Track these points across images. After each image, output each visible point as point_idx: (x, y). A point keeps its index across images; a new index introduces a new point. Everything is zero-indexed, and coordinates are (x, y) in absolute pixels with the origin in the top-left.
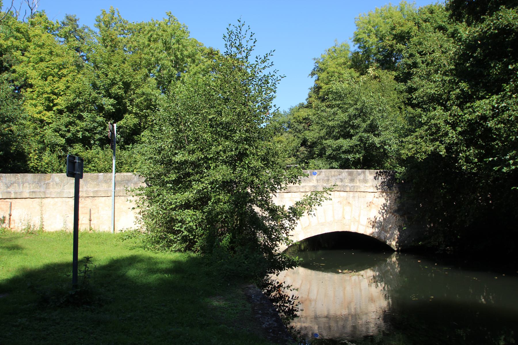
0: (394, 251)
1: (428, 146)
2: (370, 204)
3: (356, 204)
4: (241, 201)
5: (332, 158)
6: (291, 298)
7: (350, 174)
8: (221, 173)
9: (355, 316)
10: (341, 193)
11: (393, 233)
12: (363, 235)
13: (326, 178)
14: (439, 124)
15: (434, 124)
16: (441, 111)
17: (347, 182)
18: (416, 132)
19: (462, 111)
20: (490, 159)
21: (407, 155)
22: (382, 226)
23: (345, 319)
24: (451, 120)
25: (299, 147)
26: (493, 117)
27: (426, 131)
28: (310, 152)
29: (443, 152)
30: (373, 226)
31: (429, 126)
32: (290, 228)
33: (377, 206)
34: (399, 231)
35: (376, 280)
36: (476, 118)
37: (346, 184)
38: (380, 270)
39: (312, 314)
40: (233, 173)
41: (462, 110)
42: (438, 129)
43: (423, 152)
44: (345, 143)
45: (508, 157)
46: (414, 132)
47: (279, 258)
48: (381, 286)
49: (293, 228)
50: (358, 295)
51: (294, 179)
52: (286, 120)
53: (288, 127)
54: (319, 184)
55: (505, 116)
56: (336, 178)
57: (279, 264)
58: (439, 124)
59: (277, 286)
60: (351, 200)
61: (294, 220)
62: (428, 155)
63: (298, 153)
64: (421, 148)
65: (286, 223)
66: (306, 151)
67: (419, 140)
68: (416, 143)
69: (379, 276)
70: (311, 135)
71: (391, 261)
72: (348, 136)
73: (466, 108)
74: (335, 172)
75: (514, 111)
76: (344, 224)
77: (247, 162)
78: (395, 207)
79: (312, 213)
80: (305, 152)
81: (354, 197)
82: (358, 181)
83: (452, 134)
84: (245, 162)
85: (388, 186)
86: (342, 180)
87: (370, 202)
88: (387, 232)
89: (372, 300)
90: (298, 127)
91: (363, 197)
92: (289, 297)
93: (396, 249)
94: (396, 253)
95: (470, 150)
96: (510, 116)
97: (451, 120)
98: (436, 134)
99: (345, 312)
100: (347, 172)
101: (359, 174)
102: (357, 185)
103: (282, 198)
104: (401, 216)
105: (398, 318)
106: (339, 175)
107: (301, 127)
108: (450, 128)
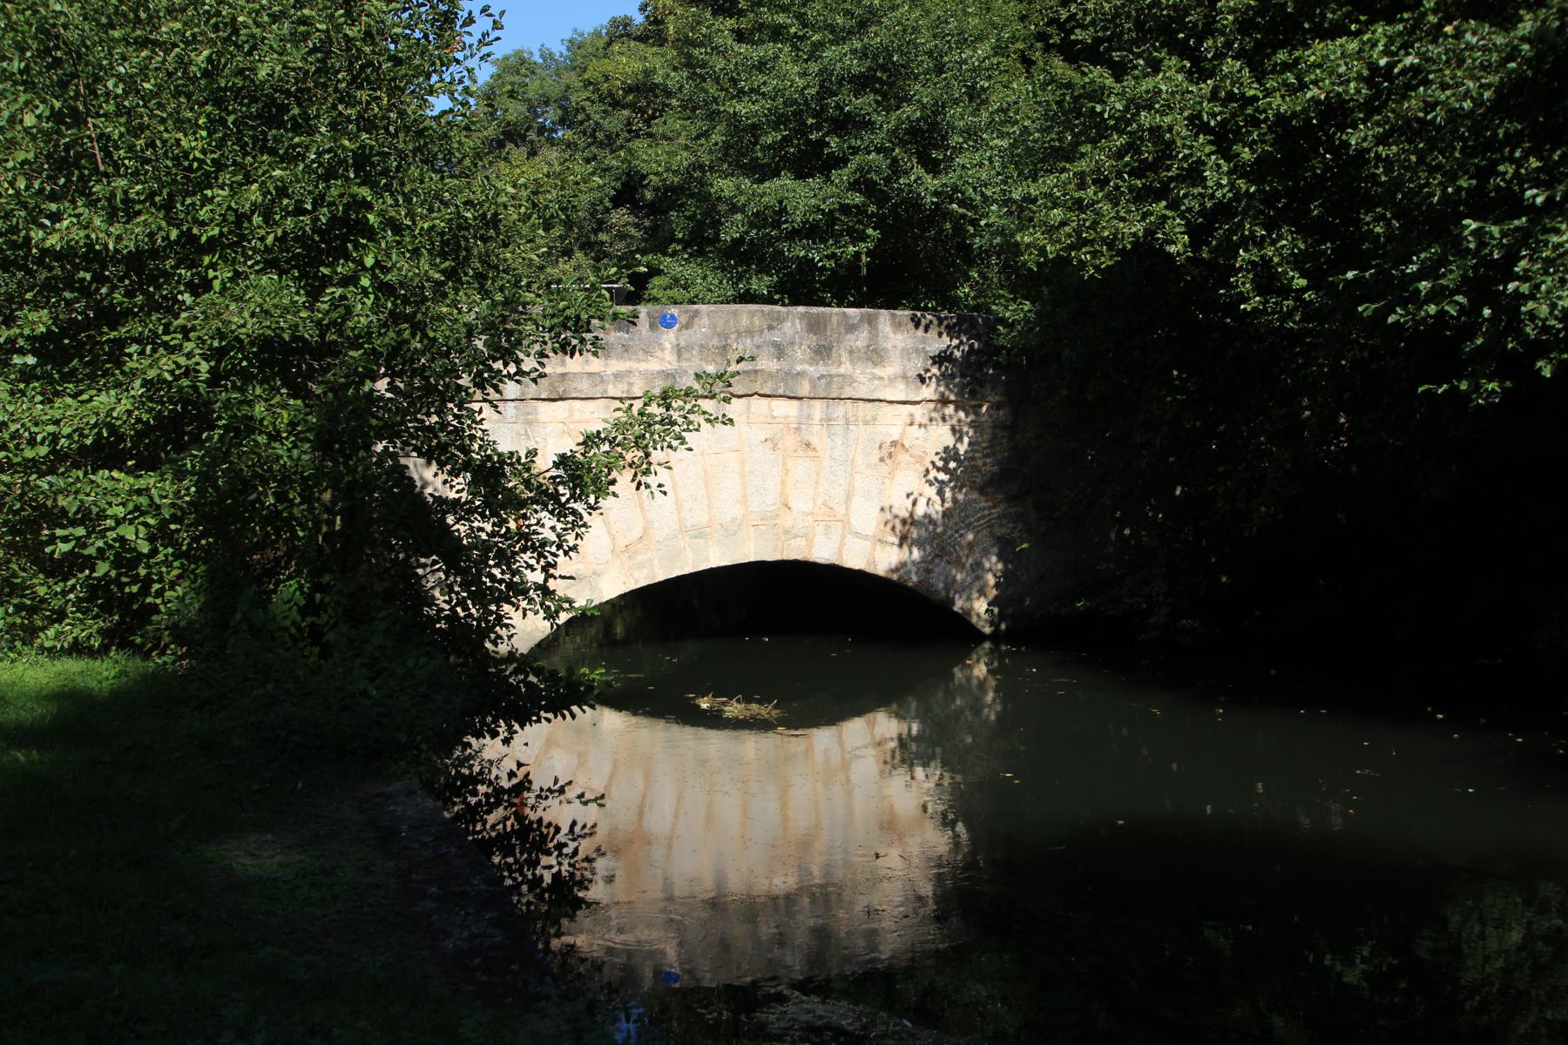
0: (980, 637)
1: (1123, 220)
2: (892, 451)
3: (828, 450)
4: (344, 429)
7: (815, 326)
10: (775, 402)
11: (978, 565)
12: (860, 573)
13: (715, 342)
15: (1151, 130)
16: (1180, 77)
19: (1259, 81)
20: (1350, 275)
24: (1214, 115)
25: (607, 210)
27: (1119, 155)
30: (903, 539)
32: (559, 547)
33: (920, 459)
35: (908, 754)
38: (924, 715)
42: (1166, 150)
43: (1104, 240)
44: (801, 196)
46: (1071, 160)
49: (574, 548)
51: (571, 333)
54: (685, 364)
55: (1412, 104)
58: (1170, 129)
60: (817, 435)
61: (574, 512)
64: (1095, 223)
65: (546, 525)
66: (637, 226)
67: (1091, 191)
68: (1079, 201)
70: (660, 157)
71: (969, 679)
73: (1273, 71)
74: (752, 314)
76: (786, 532)
77: (369, 261)
78: (988, 466)
79: (651, 479)
80: (633, 231)
81: (827, 421)
82: (845, 357)
84: (361, 263)
86: (780, 351)
87: (894, 444)
90: (605, 123)
91: (866, 423)
93: (987, 630)
94: (987, 645)
95: (1280, 237)
98: (1153, 171)
99: (783, 882)
100: (803, 316)
101: (851, 328)
102: (842, 370)
103: (530, 423)
106: (770, 328)
107: (615, 122)
108: (1208, 149)
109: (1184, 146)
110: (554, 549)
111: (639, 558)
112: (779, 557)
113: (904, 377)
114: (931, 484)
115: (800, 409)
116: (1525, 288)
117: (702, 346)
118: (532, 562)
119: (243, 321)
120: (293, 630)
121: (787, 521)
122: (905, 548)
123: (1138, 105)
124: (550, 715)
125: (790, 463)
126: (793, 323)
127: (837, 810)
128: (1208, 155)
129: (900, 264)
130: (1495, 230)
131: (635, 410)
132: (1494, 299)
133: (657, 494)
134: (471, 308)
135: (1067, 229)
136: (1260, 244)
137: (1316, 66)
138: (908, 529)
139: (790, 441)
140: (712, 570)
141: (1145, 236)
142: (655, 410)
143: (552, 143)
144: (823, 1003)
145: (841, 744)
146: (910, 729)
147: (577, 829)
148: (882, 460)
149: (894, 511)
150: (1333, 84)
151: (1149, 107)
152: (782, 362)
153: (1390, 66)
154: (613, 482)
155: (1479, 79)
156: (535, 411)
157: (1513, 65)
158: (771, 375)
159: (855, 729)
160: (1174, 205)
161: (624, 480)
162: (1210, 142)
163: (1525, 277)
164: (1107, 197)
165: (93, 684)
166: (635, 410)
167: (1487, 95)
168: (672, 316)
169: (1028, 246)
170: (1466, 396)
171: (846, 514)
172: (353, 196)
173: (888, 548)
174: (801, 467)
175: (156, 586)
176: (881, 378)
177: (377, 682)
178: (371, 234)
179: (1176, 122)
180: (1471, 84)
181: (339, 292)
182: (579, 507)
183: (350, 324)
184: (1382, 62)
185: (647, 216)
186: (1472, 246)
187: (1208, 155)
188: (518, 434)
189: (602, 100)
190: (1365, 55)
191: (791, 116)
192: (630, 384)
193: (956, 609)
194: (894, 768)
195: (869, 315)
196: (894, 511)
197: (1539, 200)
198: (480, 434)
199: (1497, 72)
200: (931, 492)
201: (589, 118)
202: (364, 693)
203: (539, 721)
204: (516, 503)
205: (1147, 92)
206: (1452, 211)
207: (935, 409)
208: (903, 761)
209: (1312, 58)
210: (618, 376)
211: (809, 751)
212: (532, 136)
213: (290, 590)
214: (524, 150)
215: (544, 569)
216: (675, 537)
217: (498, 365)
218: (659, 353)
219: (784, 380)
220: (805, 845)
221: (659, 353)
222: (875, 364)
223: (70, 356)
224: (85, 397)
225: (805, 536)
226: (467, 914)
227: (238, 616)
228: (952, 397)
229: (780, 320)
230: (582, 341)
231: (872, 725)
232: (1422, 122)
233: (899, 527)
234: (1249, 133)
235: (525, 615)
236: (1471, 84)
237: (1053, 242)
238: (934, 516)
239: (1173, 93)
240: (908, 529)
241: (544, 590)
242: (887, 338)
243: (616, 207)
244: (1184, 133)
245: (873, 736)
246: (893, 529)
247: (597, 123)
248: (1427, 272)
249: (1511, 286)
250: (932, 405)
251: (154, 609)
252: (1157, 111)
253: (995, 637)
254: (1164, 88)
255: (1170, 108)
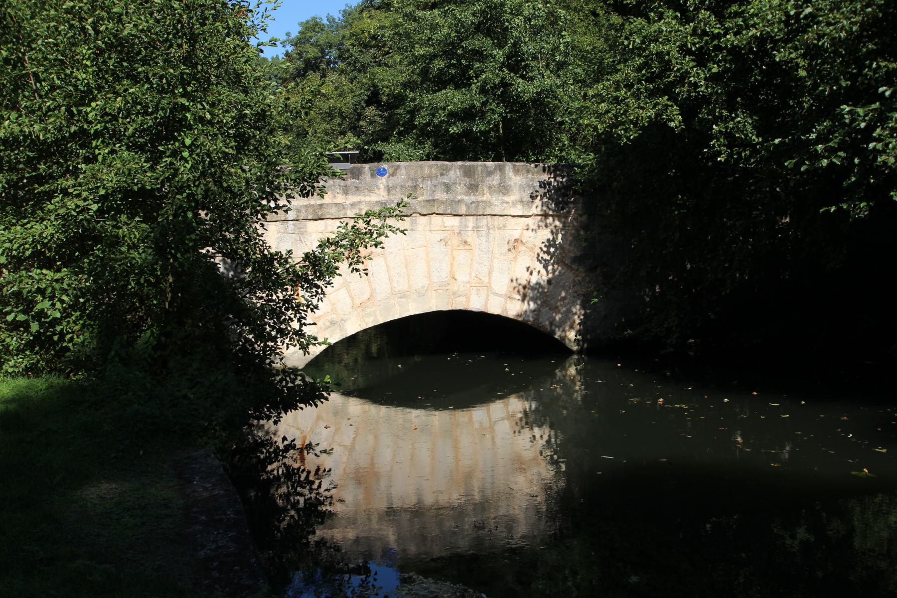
0: (570, 352)
1: (642, 108)
2: (515, 245)
3: (477, 245)
4: (175, 240)
5: (424, 133)
6: (313, 473)
7: (468, 173)
8: (116, 168)
9: (483, 506)
10: (446, 218)
11: (569, 311)
12: (498, 316)
13: (410, 183)
14: (668, 53)
15: (658, 54)
16: (674, 22)
17: (460, 193)
18: (617, 71)
19: (721, 23)
20: (777, 141)
21: (595, 129)
22: (541, 295)
23: (458, 512)
24: (694, 44)
25: (363, 108)
26: (786, 41)
27: (639, 69)
28: (388, 119)
29: (676, 122)
30: (524, 297)
31: (646, 57)
32: (308, 306)
33: (532, 249)
34: (583, 307)
35: (529, 420)
36: (749, 43)
37: (459, 198)
38: (538, 398)
39: (382, 505)
40: (152, 169)
41: (721, 18)
42: (666, 66)
43: (631, 121)
44: (454, 98)
45: (813, 136)
46: (611, 73)
47: (281, 381)
48: (542, 434)
49: (316, 307)
50: (492, 453)
51: (307, 183)
52: (335, 38)
53: (340, 57)
54: (392, 197)
55: (810, 36)
56: (434, 182)
57: (305, 391)
58: (668, 53)
59: (281, 447)
60: (470, 236)
61: (318, 287)
62: (643, 128)
63: (362, 123)
64: (626, 111)
65: (302, 295)
66: (381, 116)
67: (623, 92)
68: (617, 98)
69: (537, 411)
70: (391, 76)
71: (565, 376)
72: (461, 81)
73: (730, 17)
74: (431, 167)
75: (829, 24)
76: (454, 294)
77: (188, 142)
78: (575, 252)
79: (360, 266)
80: (378, 119)
81: (477, 228)
82: (486, 190)
83: (698, 76)
84: (183, 143)
85: (559, 199)
86: (448, 188)
87: (516, 241)
88: (556, 309)
89: (519, 464)
90: (361, 58)
91: (499, 229)
92: (309, 472)
93: (575, 348)
94: (575, 357)
95: (737, 116)
96: (820, 37)
97: (694, 44)
98: (659, 79)
99: (455, 497)
100: (461, 167)
101: (490, 174)
102: (485, 198)
103: (302, 233)
104: (591, 269)
105: (585, 502)
106: (442, 174)
107: (366, 58)
108: (691, 64)
109: (677, 63)
110: (305, 308)
111: (368, 310)
112: (450, 308)
113: (521, 201)
114: (541, 262)
115: (461, 222)
116: (880, 146)
117: (402, 186)
118: (292, 316)
119: (110, 179)
120: (149, 360)
121: (455, 287)
122: (526, 302)
123: (649, 39)
124: (302, 405)
125: (455, 253)
126: (455, 171)
127: (492, 453)
128: (692, 68)
129: (515, 136)
130: (860, 111)
131: (349, 227)
132: (864, 154)
133: (363, 275)
134: (250, 167)
135: (610, 115)
136: (725, 120)
137: (753, 15)
138: (526, 291)
139: (455, 241)
140: (411, 316)
141: (656, 117)
142: (361, 225)
143: (334, 70)
144: (435, 583)
145: (489, 415)
146: (531, 407)
147: (320, 472)
148: (509, 250)
149: (519, 281)
150: (764, 26)
151: (656, 41)
152: (449, 195)
153: (797, 14)
154: (337, 268)
155: (849, 19)
156: (305, 226)
157: (870, 9)
158: (442, 202)
159: (497, 408)
160: (673, 98)
161: (343, 267)
162: (693, 60)
163: (879, 140)
164: (633, 95)
165: (33, 394)
166: (349, 227)
167: (855, 28)
168: (384, 169)
169: (587, 125)
170: (847, 212)
171: (489, 283)
172: (176, 103)
173: (514, 302)
174: (462, 255)
175: (69, 336)
176: (507, 203)
177: (194, 390)
178: (190, 128)
179: (672, 49)
180: (845, 22)
181: (169, 160)
182: (320, 283)
183: (177, 179)
184: (792, 13)
185: (386, 111)
186: (847, 121)
187: (692, 68)
188: (295, 240)
189: (360, 45)
190: (783, 7)
191: (449, 50)
192: (360, 209)
193: (556, 337)
194: (523, 428)
195: (500, 165)
196: (519, 281)
197: (887, 94)
198: (261, 243)
199: (860, 15)
200: (540, 267)
201: (351, 55)
202: (185, 397)
203: (296, 409)
204: (279, 284)
205: (655, 32)
206: (838, 98)
207: (541, 221)
208: (527, 423)
209: (752, 11)
210: (353, 205)
211: (471, 418)
212: (323, 66)
213: (146, 335)
214: (318, 74)
215: (299, 320)
216: (389, 298)
217: (264, 202)
218: (377, 191)
219: (451, 205)
220: (469, 476)
221: (377, 191)
222: (504, 194)
223: (20, 202)
224: (29, 226)
225: (465, 295)
226: (219, 533)
227: (113, 353)
228: (551, 213)
229: (448, 170)
230: (313, 187)
231: (507, 406)
232: (816, 45)
233: (522, 290)
234: (716, 56)
235: (288, 348)
236: (845, 22)
237: (602, 123)
238: (542, 283)
239: (670, 32)
240: (526, 291)
241: (299, 333)
242: (510, 179)
243: (368, 106)
244: (677, 55)
245: (508, 412)
246: (518, 292)
247: (356, 58)
248: (823, 138)
249: (871, 146)
250: (539, 218)
251: (67, 349)
252: (661, 43)
253: (579, 352)
254: (664, 29)
255: (669, 41)
